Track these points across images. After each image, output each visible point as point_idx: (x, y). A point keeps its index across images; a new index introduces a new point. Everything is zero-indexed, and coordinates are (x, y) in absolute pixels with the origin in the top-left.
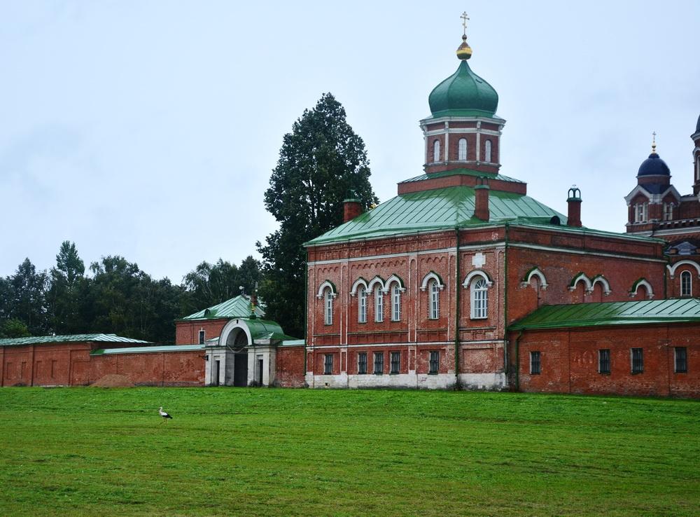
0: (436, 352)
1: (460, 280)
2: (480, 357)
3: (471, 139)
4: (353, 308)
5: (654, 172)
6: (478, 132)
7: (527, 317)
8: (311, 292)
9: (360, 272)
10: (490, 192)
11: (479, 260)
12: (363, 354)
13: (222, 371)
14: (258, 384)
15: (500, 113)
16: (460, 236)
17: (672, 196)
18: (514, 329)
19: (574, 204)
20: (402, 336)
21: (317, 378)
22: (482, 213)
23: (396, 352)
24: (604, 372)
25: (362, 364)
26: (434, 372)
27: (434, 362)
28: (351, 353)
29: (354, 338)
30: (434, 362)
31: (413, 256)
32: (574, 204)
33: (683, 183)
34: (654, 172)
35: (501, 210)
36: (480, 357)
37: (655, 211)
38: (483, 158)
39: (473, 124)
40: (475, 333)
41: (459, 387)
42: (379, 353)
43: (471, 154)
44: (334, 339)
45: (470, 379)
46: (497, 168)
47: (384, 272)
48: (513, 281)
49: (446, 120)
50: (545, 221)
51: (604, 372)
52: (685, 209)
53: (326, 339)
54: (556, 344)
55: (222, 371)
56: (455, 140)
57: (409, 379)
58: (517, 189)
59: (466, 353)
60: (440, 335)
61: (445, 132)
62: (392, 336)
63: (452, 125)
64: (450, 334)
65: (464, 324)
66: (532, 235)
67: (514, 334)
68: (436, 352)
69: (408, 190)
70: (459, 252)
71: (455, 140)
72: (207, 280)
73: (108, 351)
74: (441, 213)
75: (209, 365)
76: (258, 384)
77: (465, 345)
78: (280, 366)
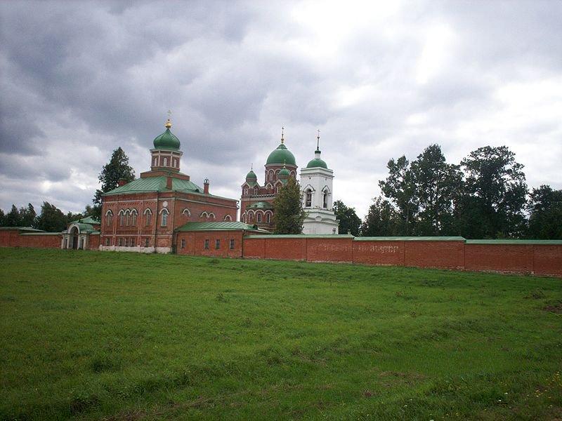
0: (148, 238)
1: (158, 211)
2: (163, 241)
3: (168, 158)
4: (118, 221)
5: (252, 178)
6: (172, 155)
7: (182, 226)
8: (103, 214)
9: (122, 207)
10: (173, 179)
11: (165, 204)
12: (121, 239)
13: (68, 243)
14: (81, 249)
15: (181, 150)
16: (159, 194)
17: (257, 186)
18: (182, 230)
19: (206, 185)
20: (136, 232)
21: (104, 247)
22: (169, 186)
23: (133, 238)
24: (207, 248)
25: (121, 242)
26: (146, 246)
27: (147, 242)
28: (117, 237)
29: (119, 232)
30: (147, 242)
31: (142, 201)
32: (206, 185)
33: (261, 182)
34: (252, 178)
35: (177, 186)
36: (163, 241)
37: (251, 191)
38: (173, 165)
39: (170, 153)
40: (162, 232)
41: (155, 252)
42: (127, 238)
43: (168, 164)
44: (110, 232)
45: (160, 250)
46: (179, 170)
47: (131, 207)
48: (176, 213)
49: (159, 150)
50: (193, 191)
51: (207, 248)
52: (261, 191)
53: (107, 233)
54: (191, 237)
55: (68, 243)
56: (162, 158)
57: (137, 249)
58: (186, 178)
59: (159, 240)
60: (150, 232)
61: (159, 155)
62: (132, 232)
63: (161, 152)
64: (154, 232)
65: (158, 228)
66: (186, 195)
67: (176, 233)
68: (148, 238)
69: (144, 176)
70: (158, 201)
71: (162, 158)
72: (528, 217)
73: (252, 236)
74: (155, 185)
75: (63, 241)
76: (81, 249)
77: (159, 236)
78: (90, 241)
